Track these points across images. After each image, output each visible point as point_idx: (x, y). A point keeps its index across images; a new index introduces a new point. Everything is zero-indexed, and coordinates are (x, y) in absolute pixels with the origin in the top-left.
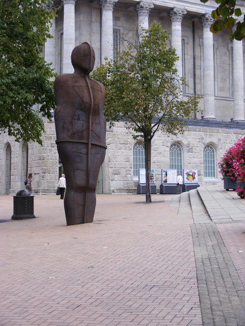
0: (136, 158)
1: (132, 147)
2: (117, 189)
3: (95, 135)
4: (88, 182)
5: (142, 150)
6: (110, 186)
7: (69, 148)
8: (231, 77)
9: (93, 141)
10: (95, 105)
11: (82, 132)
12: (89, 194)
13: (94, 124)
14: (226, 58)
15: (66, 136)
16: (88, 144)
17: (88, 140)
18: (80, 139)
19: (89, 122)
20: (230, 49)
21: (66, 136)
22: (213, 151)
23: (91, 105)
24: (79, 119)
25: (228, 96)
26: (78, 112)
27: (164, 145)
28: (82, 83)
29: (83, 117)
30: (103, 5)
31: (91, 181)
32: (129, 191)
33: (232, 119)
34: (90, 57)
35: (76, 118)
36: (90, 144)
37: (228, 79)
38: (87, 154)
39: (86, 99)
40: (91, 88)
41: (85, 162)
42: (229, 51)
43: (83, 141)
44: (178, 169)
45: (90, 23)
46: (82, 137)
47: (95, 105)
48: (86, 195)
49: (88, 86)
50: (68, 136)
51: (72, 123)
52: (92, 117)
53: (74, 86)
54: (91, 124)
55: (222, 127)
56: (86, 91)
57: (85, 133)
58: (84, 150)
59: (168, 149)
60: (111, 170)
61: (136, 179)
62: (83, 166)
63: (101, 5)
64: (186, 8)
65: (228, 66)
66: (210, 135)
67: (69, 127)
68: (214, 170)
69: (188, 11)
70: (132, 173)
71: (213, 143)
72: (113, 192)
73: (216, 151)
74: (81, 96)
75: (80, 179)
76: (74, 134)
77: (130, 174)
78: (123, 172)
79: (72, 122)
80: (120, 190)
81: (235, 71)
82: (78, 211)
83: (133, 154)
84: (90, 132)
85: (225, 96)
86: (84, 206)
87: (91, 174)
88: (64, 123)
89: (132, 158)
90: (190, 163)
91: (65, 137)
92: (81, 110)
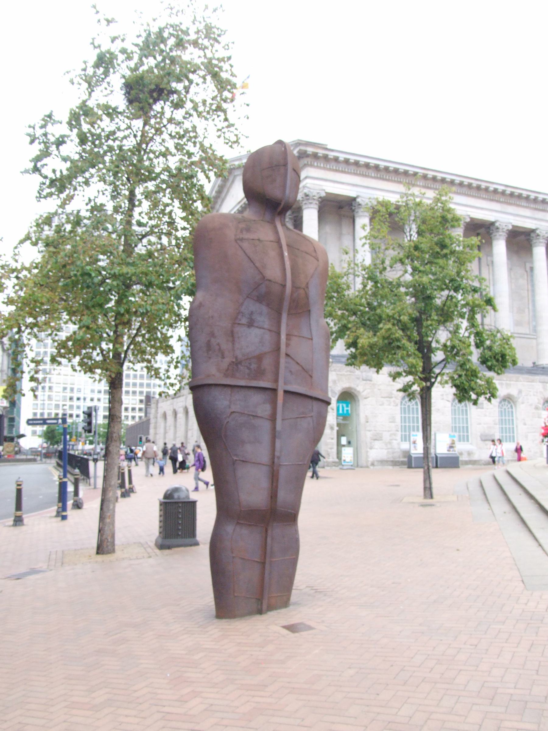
0: (405, 417)
1: (398, 401)
2: (378, 461)
3: (295, 368)
4: (273, 495)
5: (416, 405)
6: (367, 457)
7: (222, 402)
8: (531, 307)
9: (288, 382)
10: (295, 287)
11: (259, 358)
12: (277, 531)
13: (294, 341)
14: (523, 282)
15: (213, 370)
16: (274, 391)
17: (276, 381)
18: (255, 378)
19: (279, 334)
20: (528, 269)
21: (213, 370)
22: (511, 406)
23: (284, 286)
24: (251, 324)
25: (528, 332)
26: (251, 306)
27: (443, 399)
28: (264, 233)
29: (264, 320)
30: (356, 210)
31: (283, 495)
32: (395, 463)
33: (534, 363)
34: (286, 170)
35: (244, 321)
36: (280, 393)
37: (527, 310)
38: (273, 418)
39: (273, 272)
40: (288, 246)
41: (266, 438)
42: (527, 272)
43: (262, 384)
44: (459, 432)
45: (340, 237)
46: (259, 373)
47: (298, 288)
48: (269, 532)
49: (278, 241)
50: (219, 370)
51: (232, 335)
52: (287, 325)
53: (242, 240)
54: (283, 337)
55: (522, 373)
56: (273, 254)
57: (267, 363)
58: (265, 410)
59: (449, 404)
60: (369, 434)
61: (405, 446)
62: (262, 454)
63: (353, 211)
64: (469, 213)
65: (526, 292)
66: (507, 384)
67: (224, 346)
68: (513, 432)
69: (472, 219)
70: (399, 438)
71: (513, 396)
72: (373, 464)
73: (515, 406)
74: (258, 264)
75: (253, 491)
76: (236, 364)
77: (396, 440)
78: (386, 436)
79: (232, 332)
80: (383, 462)
81: (537, 298)
82: (245, 576)
83: (399, 411)
84: (283, 360)
85: (524, 332)
86: (263, 563)
87: (283, 473)
88: (212, 335)
89: (398, 419)
90: (480, 424)
91: (213, 372)
92: (260, 299)
